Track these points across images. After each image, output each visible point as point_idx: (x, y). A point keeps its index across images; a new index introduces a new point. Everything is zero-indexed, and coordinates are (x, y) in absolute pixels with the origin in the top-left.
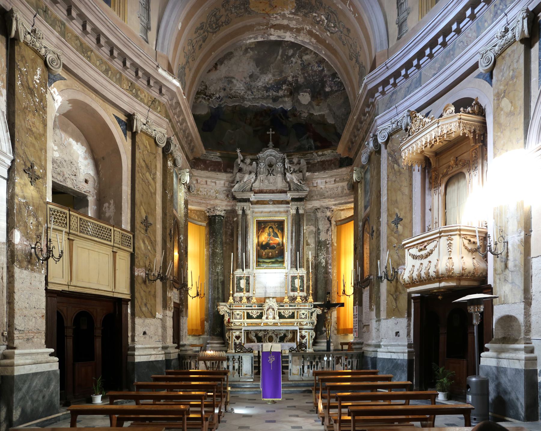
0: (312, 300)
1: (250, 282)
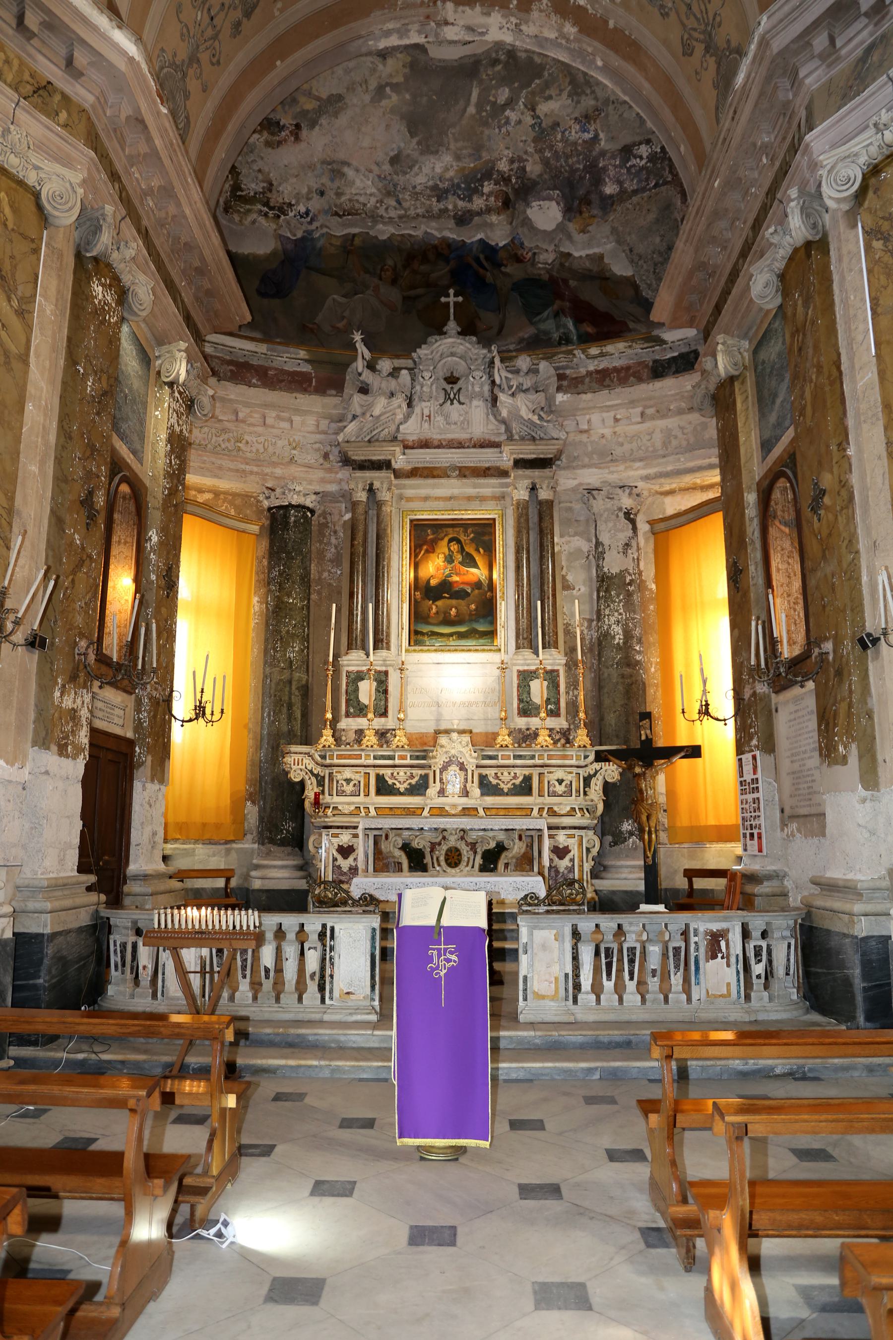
0: (586, 741)
1: (390, 689)
